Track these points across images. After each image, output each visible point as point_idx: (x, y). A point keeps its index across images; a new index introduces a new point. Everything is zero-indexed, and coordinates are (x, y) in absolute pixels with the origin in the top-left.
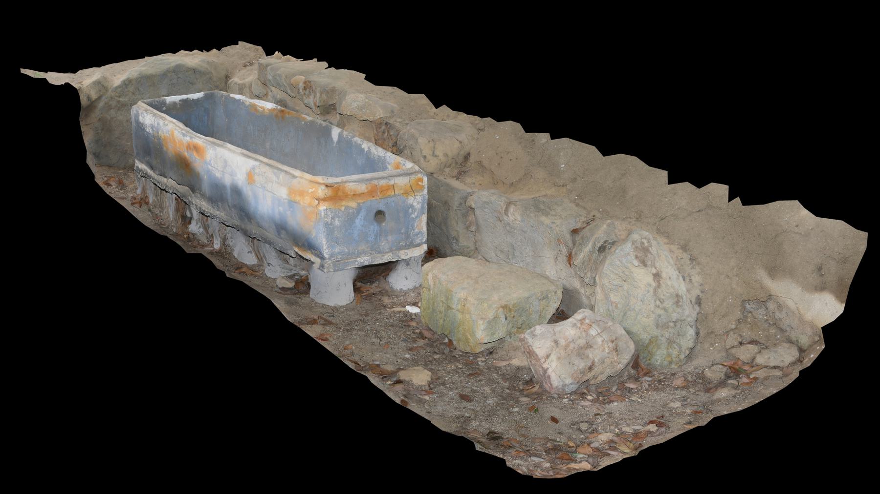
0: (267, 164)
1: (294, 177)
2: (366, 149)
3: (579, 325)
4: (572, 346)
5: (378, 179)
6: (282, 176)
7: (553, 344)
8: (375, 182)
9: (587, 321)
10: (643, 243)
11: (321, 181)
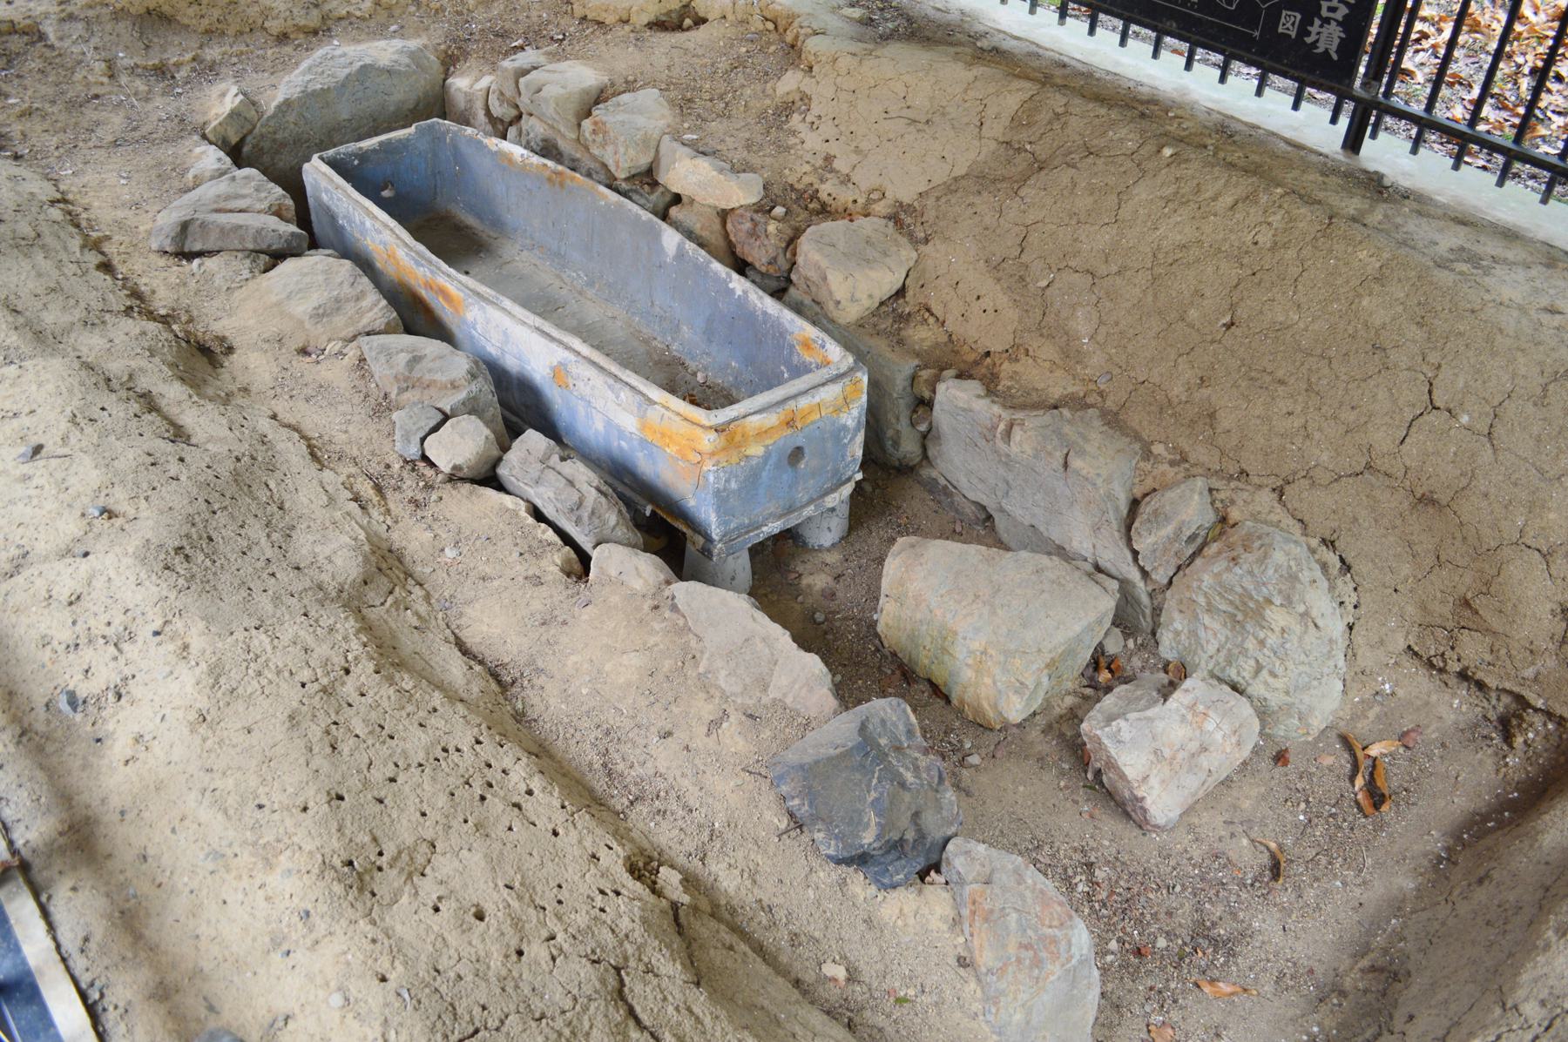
0: (594, 363)
1: (651, 402)
2: (739, 292)
3: (1189, 717)
4: (1181, 755)
5: (794, 397)
6: (625, 394)
7: (1152, 757)
8: (791, 404)
9: (1201, 708)
11: (707, 424)
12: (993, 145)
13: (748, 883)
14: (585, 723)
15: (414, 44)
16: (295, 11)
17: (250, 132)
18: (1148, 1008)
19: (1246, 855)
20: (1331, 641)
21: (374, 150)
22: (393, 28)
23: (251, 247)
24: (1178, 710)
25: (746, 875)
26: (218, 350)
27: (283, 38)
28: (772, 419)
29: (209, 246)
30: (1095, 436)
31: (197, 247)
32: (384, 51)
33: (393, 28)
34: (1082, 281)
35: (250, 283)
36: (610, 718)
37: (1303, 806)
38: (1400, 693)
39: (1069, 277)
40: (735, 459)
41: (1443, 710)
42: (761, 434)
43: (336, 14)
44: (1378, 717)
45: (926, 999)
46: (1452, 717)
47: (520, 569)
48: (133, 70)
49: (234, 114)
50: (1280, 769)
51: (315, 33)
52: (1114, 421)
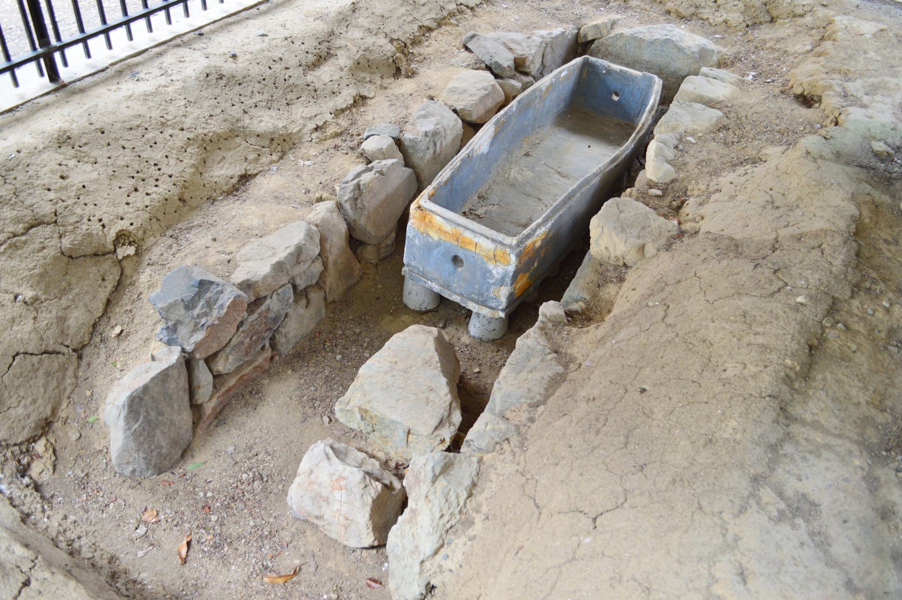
3: (334, 478)
4: (315, 487)
5: (467, 228)
8: (461, 230)
9: (343, 483)
15: (710, 45)
18: (168, 511)
20: (417, 547)
22: (718, 36)
27: (669, 12)
28: (448, 228)
30: (537, 375)
33: (718, 36)
43: (702, 16)
47: (311, 186)
49: (596, 27)
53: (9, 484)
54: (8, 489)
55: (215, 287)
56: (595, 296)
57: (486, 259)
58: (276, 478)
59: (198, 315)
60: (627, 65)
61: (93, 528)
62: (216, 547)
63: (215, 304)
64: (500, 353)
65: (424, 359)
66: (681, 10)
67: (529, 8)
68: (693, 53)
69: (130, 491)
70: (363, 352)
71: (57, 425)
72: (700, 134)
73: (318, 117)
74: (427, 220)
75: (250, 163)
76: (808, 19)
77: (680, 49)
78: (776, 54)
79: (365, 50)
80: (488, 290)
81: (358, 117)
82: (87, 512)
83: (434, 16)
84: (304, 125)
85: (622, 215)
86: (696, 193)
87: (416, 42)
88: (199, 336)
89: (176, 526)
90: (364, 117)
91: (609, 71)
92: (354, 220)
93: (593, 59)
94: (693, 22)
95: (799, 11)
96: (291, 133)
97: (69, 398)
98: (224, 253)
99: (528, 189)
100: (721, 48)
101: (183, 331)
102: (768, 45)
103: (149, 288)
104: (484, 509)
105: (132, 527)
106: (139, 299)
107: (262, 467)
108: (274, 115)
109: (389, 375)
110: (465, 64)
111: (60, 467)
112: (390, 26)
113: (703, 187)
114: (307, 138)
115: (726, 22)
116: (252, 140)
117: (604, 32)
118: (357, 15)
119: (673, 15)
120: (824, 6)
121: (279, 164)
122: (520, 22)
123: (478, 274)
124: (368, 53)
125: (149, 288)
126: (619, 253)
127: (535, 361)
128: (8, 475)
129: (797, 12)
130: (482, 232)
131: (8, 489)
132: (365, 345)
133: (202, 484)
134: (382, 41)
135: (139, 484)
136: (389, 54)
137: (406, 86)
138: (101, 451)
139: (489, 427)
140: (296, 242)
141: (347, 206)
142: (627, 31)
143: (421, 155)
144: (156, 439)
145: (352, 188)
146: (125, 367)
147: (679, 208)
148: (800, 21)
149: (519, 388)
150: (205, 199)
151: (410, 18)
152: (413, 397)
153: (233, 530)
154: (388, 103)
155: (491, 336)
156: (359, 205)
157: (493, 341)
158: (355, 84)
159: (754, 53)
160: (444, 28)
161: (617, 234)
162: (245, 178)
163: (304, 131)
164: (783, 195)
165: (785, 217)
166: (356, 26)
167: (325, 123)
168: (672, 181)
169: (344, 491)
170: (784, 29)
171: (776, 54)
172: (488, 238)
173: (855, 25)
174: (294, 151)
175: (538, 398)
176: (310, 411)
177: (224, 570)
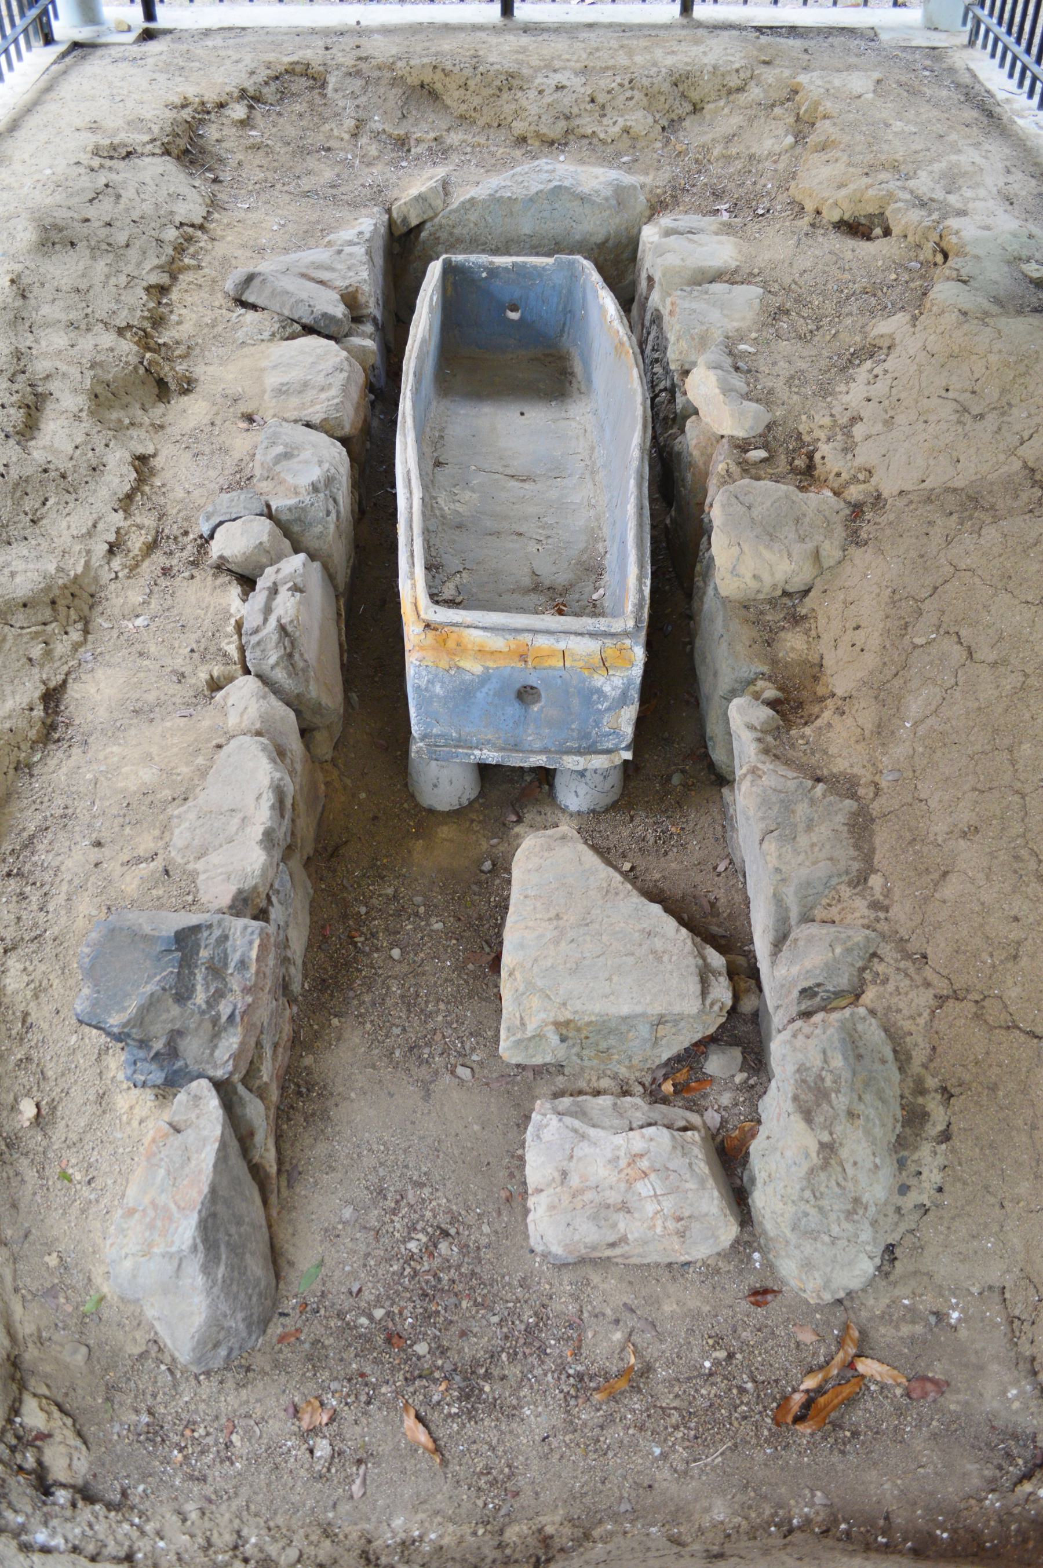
3: (623, 1163)
4: (589, 1196)
5: (535, 632)
7: (556, 1175)
8: (527, 638)
9: (644, 1164)
10: (823, 1080)
12: (1017, 465)
13: (29, 994)
14: (60, 801)
15: (629, 179)
16: (544, 118)
17: (431, 219)
18: (334, 1385)
19: (605, 1345)
20: (856, 1201)
21: (506, 269)
22: (625, 159)
23: (286, 313)
24: (618, 1148)
25: (32, 986)
26: (173, 388)
27: (522, 140)
28: (498, 643)
29: (259, 302)
30: (823, 831)
31: (251, 299)
32: (595, 177)
33: (625, 159)
34: (957, 653)
35: (264, 345)
36: (81, 807)
37: (721, 1354)
38: (963, 1333)
39: (949, 645)
40: (443, 664)
41: (990, 1389)
42: (482, 652)
43: (582, 131)
44: (913, 1340)
45: (86, 1192)
46: (995, 1404)
47: (179, 663)
48: (376, 135)
49: (421, 198)
50: (745, 1305)
51: (552, 143)
52: (861, 827)
53: (46, 1524)
54: (53, 1534)
55: (205, 934)
56: (774, 662)
57: (586, 673)
58: (471, 1219)
59: (207, 1002)
60: (496, 252)
61: (240, 1501)
62: (468, 1397)
63: (226, 965)
64: (637, 820)
65: (600, 889)
66: (544, 130)
67: (287, 198)
68: (607, 199)
69: (244, 1392)
70: (428, 925)
71: (31, 1354)
72: (754, 335)
73: (100, 526)
74: (451, 644)
75: (42, 666)
76: (755, 92)
77: (583, 199)
78: (738, 165)
79: (92, 367)
80: (597, 724)
81: (162, 500)
82: (204, 1479)
83: (156, 262)
84: (88, 552)
85: (755, 512)
86: (822, 435)
87: (158, 321)
88: (231, 1042)
89: (368, 1403)
90: (170, 495)
91: (493, 272)
92: (298, 695)
93: (459, 258)
94: (573, 146)
95: (734, 82)
96: (76, 577)
97: (16, 1290)
98: (139, 860)
99: (488, 524)
100: (642, 179)
101: (192, 1048)
102: (716, 152)
103: (36, 996)
104: (931, 1083)
105: (302, 1453)
106: (28, 1027)
107: (428, 1214)
108: (25, 552)
109: (563, 944)
110: (266, 335)
111: (91, 1430)
112: (102, 306)
113: (827, 421)
114: (106, 576)
115: (626, 131)
116: (20, 618)
117: (438, 203)
118: (33, 302)
119: (534, 144)
120: (766, 63)
121: (89, 646)
122: (291, 228)
123: (575, 702)
124: (100, 372)
125: (36, 996)
126: (780, 577)
127: (802, 809)
128: (29, 1509)
129: (731, 84)
130: (566, 628)
131: (53, 1534)
132: (422, 910)
133: (348, 1303)
134: (108, 339)
135: (248, 1369)
136: (133, 360)
137: (190, 412)
138: (143, 1356)
139: (838, 950)
140: (267, 782)
141: (280, 675)
142: (480, 192)
143: (319, 528)
144: (249, 1273)
145: (275, 637)
146: (92, 1173)
147: (810, 467)
148: (742, 98)
149: (815, 863)
150: (12, 772)
151: (123, 280)
152: (631, 960)
153: (473, 1348)
154: (188, 455)
155: (608, 800)
156: (301, 664)
157: (614, 807)
158: (114, 437)
159: (699, 172)
160: (185, 278)
161: (767, 547)
162: (52, 697)
163: (95, 562)
164: (974, 392)
165: (1005, 427)
166: (47, 325)
167: (117, 532)
168: (769, 427)
169: (653, 1176)
170: (723, 120)
171: (738, 165)
172: (581, 634)
173: (837, 82)
174: (100, 609)
175: (856, 866)
176: (423, 1072)
177: (514, 1425)
